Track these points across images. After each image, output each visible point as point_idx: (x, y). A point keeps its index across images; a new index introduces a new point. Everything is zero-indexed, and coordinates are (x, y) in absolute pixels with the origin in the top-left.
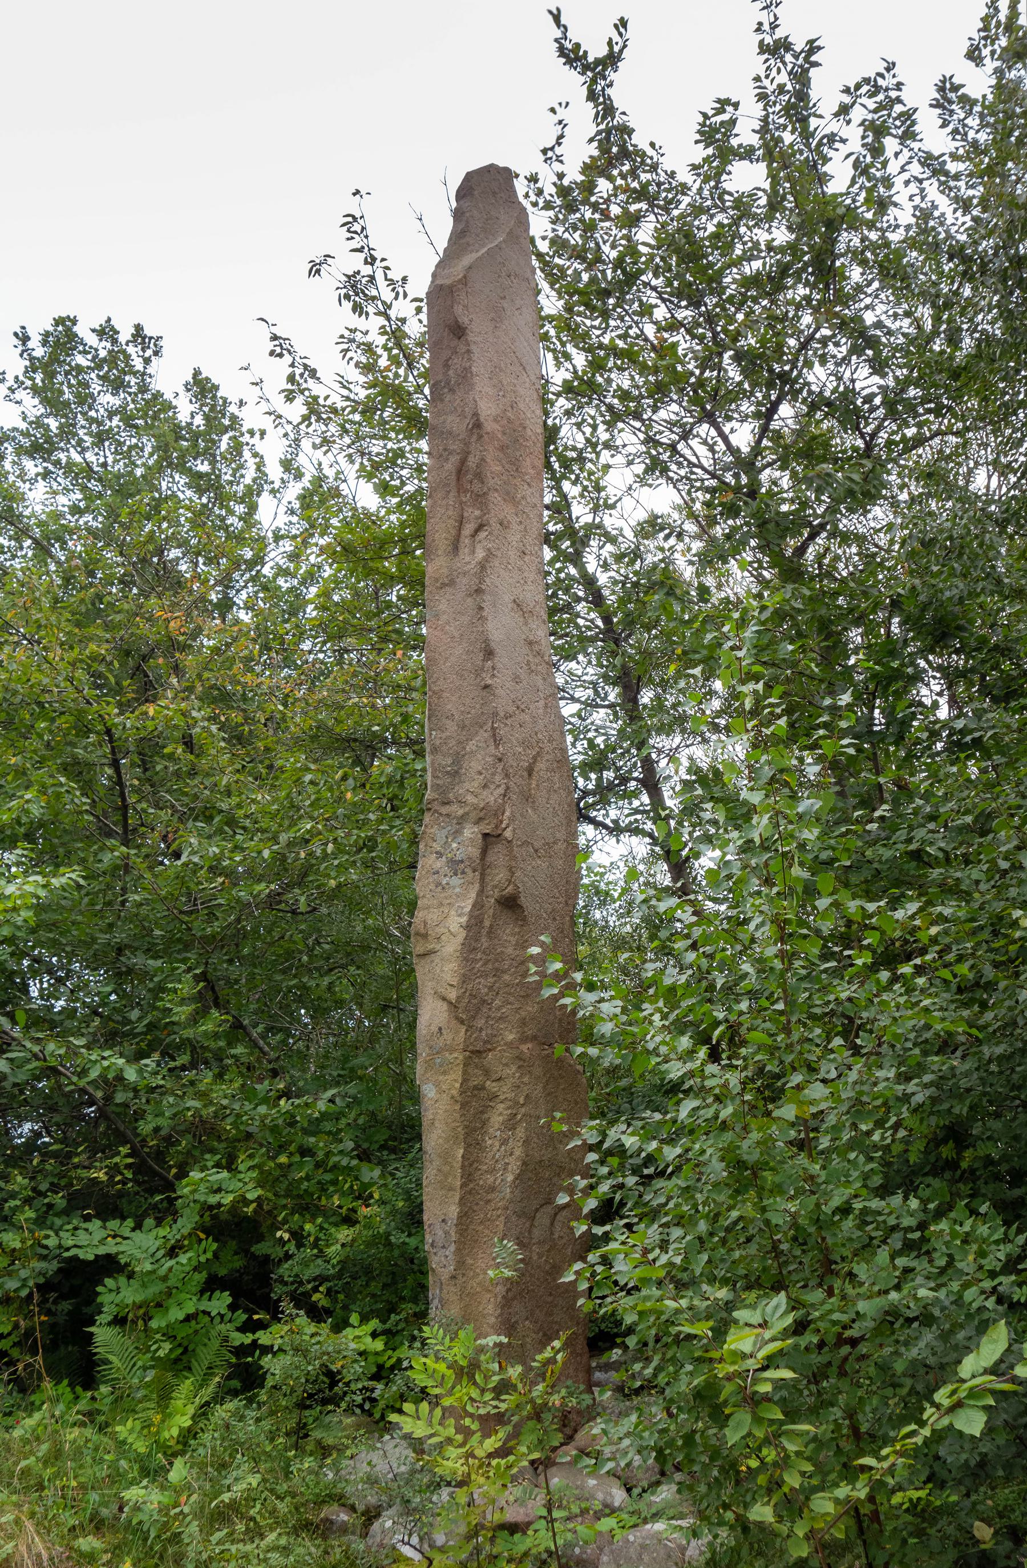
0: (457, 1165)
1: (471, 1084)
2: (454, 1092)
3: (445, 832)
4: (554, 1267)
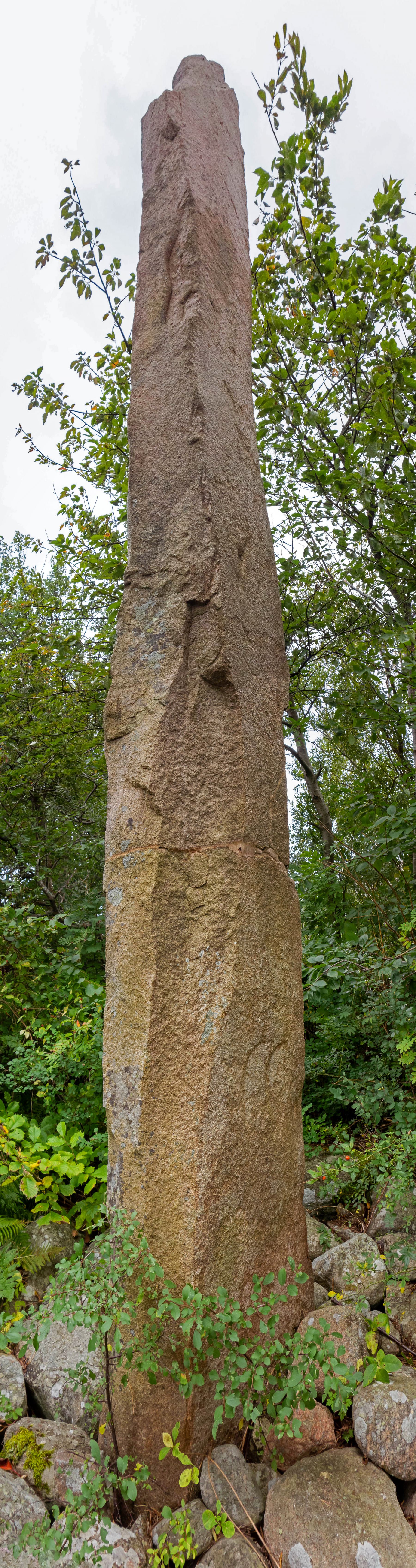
0: (147, 995)
1: (168, 889)
2: (145, 899)
4: (270, 1123)
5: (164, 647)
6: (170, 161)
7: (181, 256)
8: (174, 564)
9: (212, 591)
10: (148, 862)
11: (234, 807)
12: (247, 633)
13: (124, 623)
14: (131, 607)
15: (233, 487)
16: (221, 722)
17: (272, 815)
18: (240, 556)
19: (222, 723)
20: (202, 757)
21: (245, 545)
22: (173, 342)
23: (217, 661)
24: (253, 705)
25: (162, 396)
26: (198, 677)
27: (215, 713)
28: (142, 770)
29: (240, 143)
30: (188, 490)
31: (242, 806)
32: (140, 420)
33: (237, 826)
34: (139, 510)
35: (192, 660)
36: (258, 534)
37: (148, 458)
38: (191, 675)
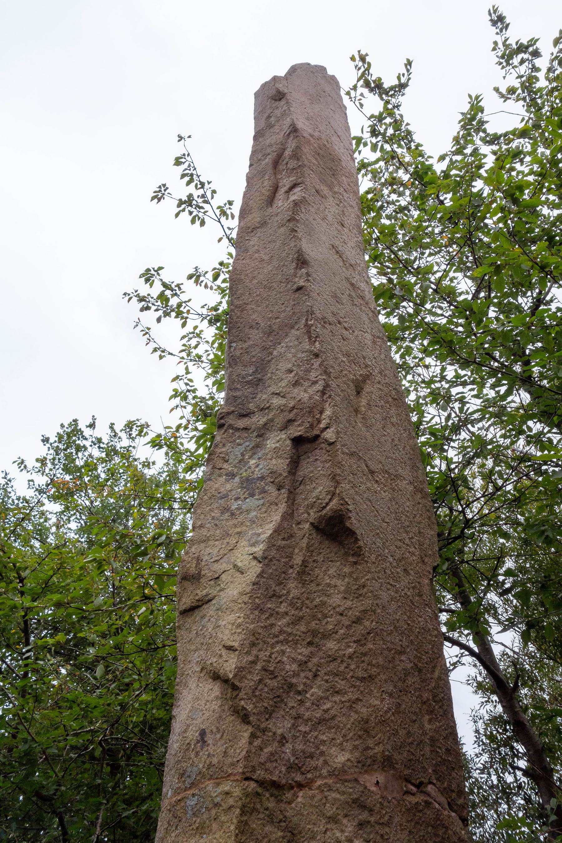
3: (238, 451)
5: (264, 491)
6: (278, 112)
7: (287, 164)
8: (277, 401)
9: (322, 426)
10: (225, 806)
11: (364, 710)
12: (372, 472)
13: (214, 467)
14: (223, 450)
15: (345, 328)
16: (339, 583)
17: (427, 726)
18: (358, 393)
19: (341, 584)
20: (314, 633)
21: (364, 381)
22: (278, 218)
23: (331, 504)
24: (384, 560)
25: (266, 258)
26: (307, 526)
27: (331, 571)
28: (224, 652)
29: (342, 102)
30: (293, 331)
31: (376, 709)
32: (243, 277)
33: (370, 743)
34: (238, 353)
35: (300, 505)
36: (380, 373)
37: (249, 307)
38: (299, 523)
